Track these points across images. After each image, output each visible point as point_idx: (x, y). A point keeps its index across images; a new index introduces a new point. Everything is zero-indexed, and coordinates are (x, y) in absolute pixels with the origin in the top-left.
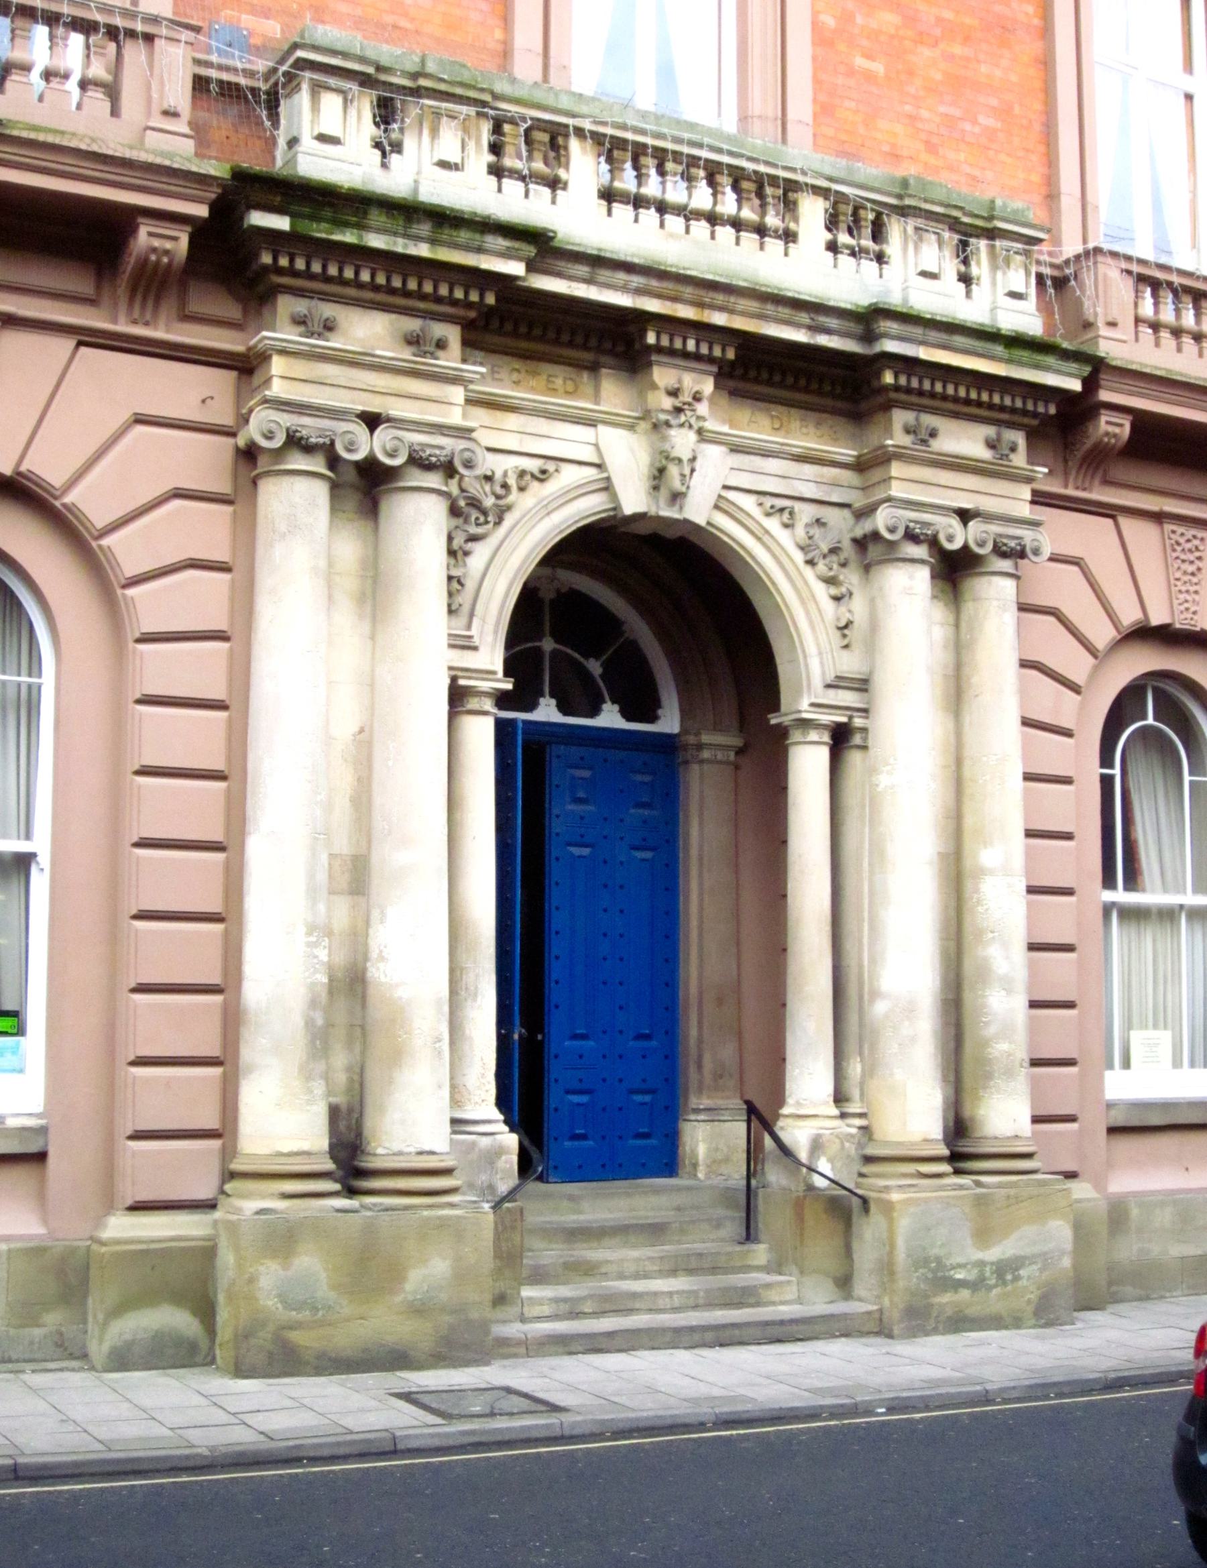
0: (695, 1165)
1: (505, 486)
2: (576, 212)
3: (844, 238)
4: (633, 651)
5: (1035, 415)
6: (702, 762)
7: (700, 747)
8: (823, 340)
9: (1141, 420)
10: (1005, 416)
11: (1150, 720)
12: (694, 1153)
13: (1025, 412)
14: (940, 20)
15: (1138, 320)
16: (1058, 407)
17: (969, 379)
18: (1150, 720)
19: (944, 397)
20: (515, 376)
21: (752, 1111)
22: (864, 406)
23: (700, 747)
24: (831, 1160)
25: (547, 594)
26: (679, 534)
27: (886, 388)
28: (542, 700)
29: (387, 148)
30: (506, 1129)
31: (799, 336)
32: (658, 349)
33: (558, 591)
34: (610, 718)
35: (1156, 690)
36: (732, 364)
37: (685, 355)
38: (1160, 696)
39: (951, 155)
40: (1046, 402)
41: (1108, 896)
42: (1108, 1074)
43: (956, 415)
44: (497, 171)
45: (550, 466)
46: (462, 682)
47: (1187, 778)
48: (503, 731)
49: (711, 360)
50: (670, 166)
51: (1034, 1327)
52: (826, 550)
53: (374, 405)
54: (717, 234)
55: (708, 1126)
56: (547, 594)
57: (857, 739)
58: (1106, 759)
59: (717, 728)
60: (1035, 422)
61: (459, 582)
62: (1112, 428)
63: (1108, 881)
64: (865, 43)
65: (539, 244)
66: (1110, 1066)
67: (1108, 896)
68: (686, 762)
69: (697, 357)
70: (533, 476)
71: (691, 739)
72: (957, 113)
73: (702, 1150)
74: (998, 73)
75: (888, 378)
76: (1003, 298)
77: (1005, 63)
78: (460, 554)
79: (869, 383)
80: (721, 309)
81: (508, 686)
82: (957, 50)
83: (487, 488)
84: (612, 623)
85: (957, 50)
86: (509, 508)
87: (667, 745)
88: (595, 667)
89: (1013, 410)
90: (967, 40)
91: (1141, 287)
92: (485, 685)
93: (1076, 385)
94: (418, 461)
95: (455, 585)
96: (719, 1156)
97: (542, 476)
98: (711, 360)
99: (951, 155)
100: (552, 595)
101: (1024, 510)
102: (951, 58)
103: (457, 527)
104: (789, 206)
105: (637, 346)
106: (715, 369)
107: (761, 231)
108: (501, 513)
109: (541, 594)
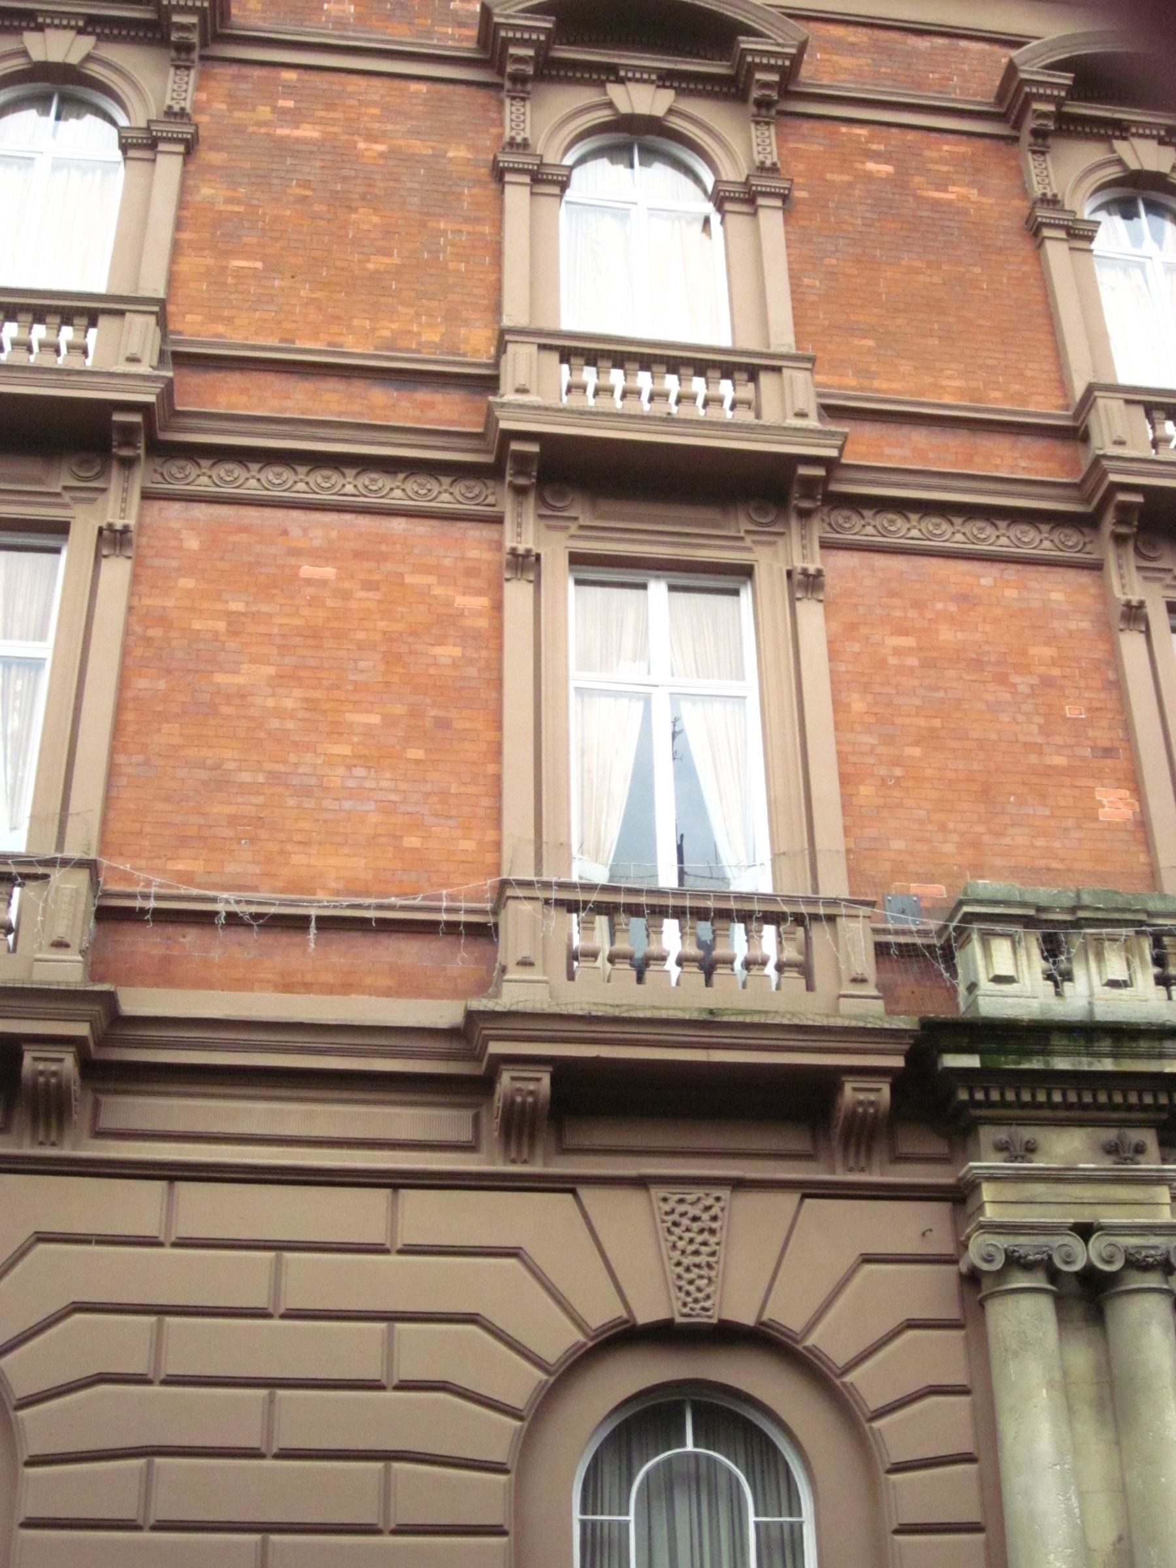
11: (690, 1447)
29: (1059, 978)
53: (1084, 1215)
60: (1165, 1116)
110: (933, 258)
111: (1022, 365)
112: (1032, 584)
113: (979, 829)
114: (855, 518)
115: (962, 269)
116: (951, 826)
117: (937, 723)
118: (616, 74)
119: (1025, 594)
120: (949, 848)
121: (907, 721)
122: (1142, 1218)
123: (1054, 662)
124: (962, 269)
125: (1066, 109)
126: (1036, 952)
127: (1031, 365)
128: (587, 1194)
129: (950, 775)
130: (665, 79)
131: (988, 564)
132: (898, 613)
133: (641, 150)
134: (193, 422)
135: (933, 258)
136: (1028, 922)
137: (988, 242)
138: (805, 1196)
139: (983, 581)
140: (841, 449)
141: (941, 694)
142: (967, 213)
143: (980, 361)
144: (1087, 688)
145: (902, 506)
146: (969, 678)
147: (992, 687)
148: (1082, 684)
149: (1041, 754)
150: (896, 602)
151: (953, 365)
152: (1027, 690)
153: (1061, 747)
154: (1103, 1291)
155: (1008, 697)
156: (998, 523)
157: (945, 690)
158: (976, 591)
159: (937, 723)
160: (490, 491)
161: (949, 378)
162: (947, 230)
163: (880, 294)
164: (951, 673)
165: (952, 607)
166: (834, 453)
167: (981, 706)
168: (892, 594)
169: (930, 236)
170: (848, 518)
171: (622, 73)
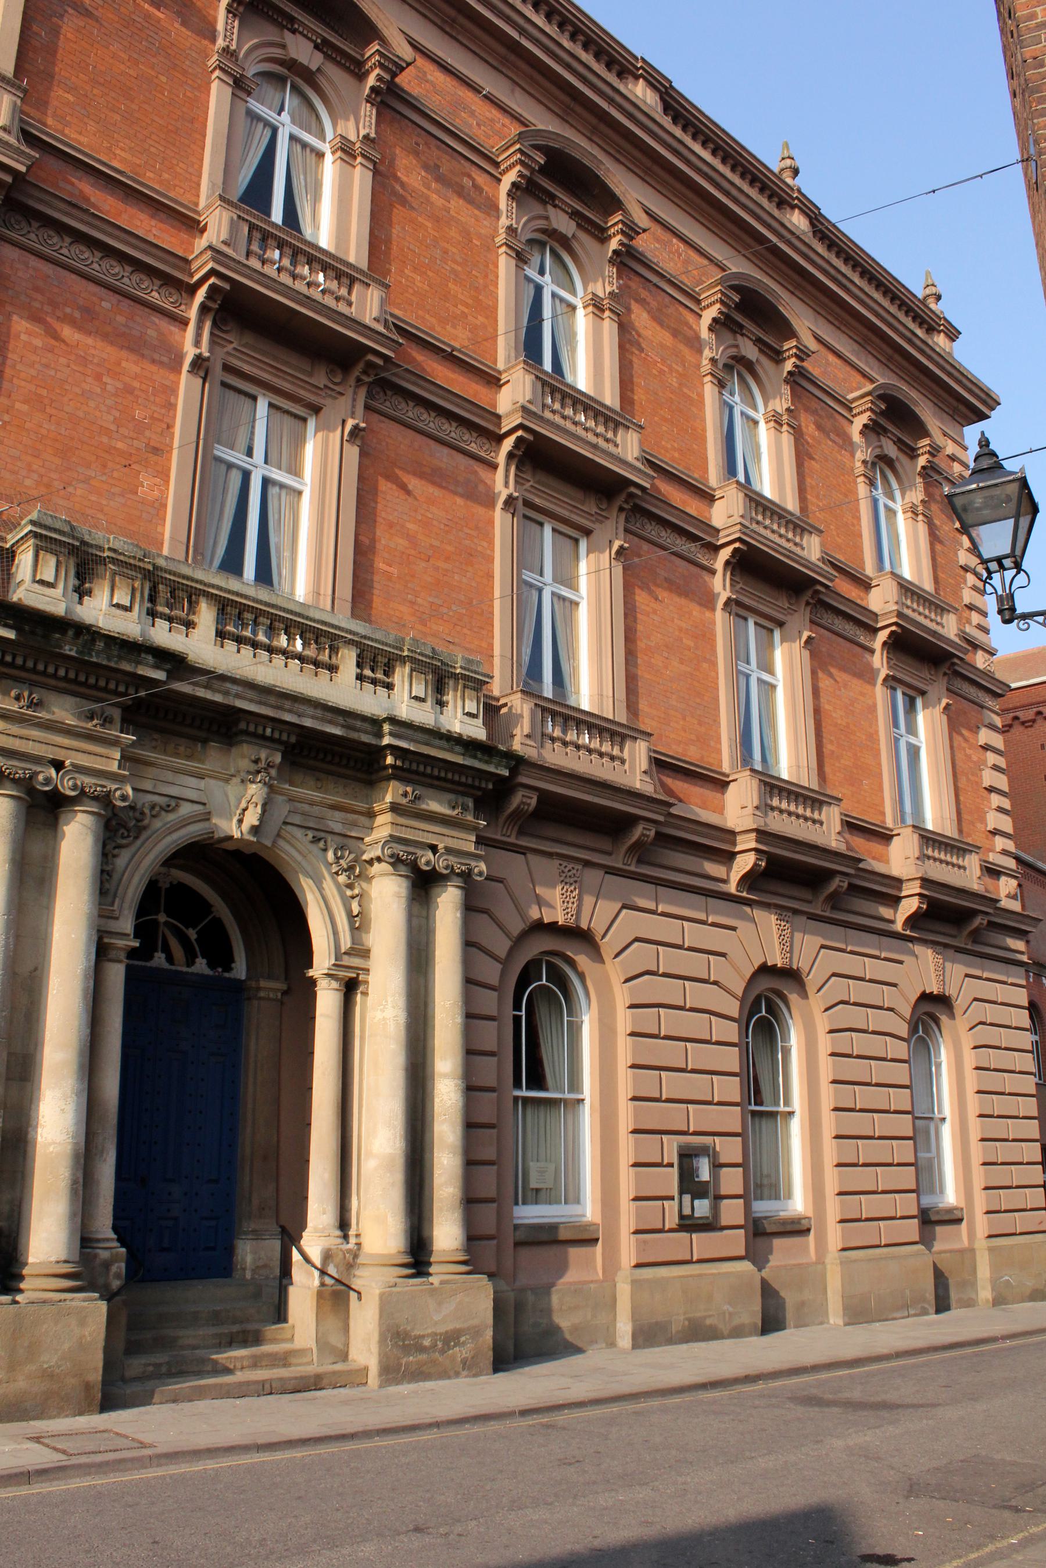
0: (244, 1269)
1: (143, 813)
2: (200, 643)
3: (367, 672)
4: (218, 924)
5: (479, 788)
6: (260, 998)
7: (259, 989)
8: (354, 735)
9: (544, 796)
10: (461, 789)
11: (544, 982)
12: (244, 1260)
13: (472, 787)
14: (432, 546)
15: (543, 735)
16: (494, 784)
17: (441, 764)
18: (544, 982)
19: (424, 775)
20: (154, 743)
21: (284, 1231)
22: (374, 777)
23: (259, 989)
24: (337, 1267)
25: (164, 885)
26: (253, 851)
27: (386, 767)
28: (156, 954)
29: (82, 592)
30: (118, 1244)
31: (337, 731)
32: (246, 733)
33: (171, 883)
34: (201, 966)
35: (548, 962)
36: (294, 746)
37: (263, 737)
38: (551, 966)
39: (435, 627)
40: (487, 781)
41: (517, 1093)
42: (515, 1208)
43: (431, 786)
44: (152, 614)
45: (173, 803)
46: (106, 940)
47: (566, 1019)
48: (131, 976)
49: (279, 741)
50: (261, 619)
51: (466, 1377)
52: (345, 867)
53: (59, 755)
54: (289, 665)
55: (254, 1242)
56: (164, 885)
57: (361, 988)
58: (517, 1007)
59: (270, 977)
60: (480, 793)
61: (108, 874)
62: (523, 800)
63: (517, 1084)
64: (386, 555)
65: (174, 662)
66: (517, 1203)
67: (517, 1093)
68: (249, 999)
69: (271, 739)
70: (161, 808)
71: (254, 984)
72: (440, 602)
73: (249, 1259)
74: (464, 580)
75: (389, 760)
76: (460, 718)
77: (469, 575)
78: (110, 857)
79: (378, 763)
80: (290, 711)
81: (136, 944)
82: (441, 564)
83: (131, 814)
84: (205, 907)
85: (441, 564)
86: (145, 828)
87: (238, 987)
88: (192, 934)
89: (465, 785)
90: (447, 559)
91: (546, 715)
92: (121, 943)
93: (506, 773)
94: (83, 794)
95: (106, 876)
96: (260, 1263)
97: (168, 809)
98: (279, 741)
99: (435, 627)
100: (168, 886)
101: (471, 848)
102: (437, 569)
103: (109, 838)
104: (334, 650)
105: (376, 766)
106: (282, 748)
107: (317, 664)
108: (140, 829)
109: (160, 885)
110: (135, 56)
111: (175, 162)
112: (138, 319)
113: (54, 476)
114: (24, 224)
115: (153, 73)
116: (35, 467)
117: (44, 392)
118: (553, 201)
119: (131, 324)
120: (28, 482)
121: (23, 383)
122: (98, 764)
123: (136, 377)
124: (153, 73)
125: (535, 178)
126: (72, 572)
127: (181, 164)
128: (530, 856)
129: (44, 432)
130: (575, 215)
131: (111, 293)
132: (37, 305)
133: (292, 86)
134: (37, 194)
135: (135, 56)
136: (73, 551)
137: (178, 62)
138: (606, 873)
139: (103, 304)
140: (29, 168)
141: (52, 373)
142: (169, 34)
143: (147, 147)
144: (154, 402)
145: (123, 258)
146: (75, 368)
147: (89, 380)
148: (152, 398)
149: (110, 438)
150: (39, 297)
151: (127, 141)
152: (113, 391)
153: (126, 437)
154: (61, 807)
155: (98, 390)
156: (32, 222)
157: (56, 371)
158: (97, 308)
159: (44, 392)
160: (184, 302)
161: (122, 149)
162: (150, 39)
163: (88, 65)
164: (63, 361)
165: (77, 314)
166: (23, 169)
167: (78, 391)
168: (37, 289)
169: (137, 38)
170: (19, 222)
171: (557, 202)
